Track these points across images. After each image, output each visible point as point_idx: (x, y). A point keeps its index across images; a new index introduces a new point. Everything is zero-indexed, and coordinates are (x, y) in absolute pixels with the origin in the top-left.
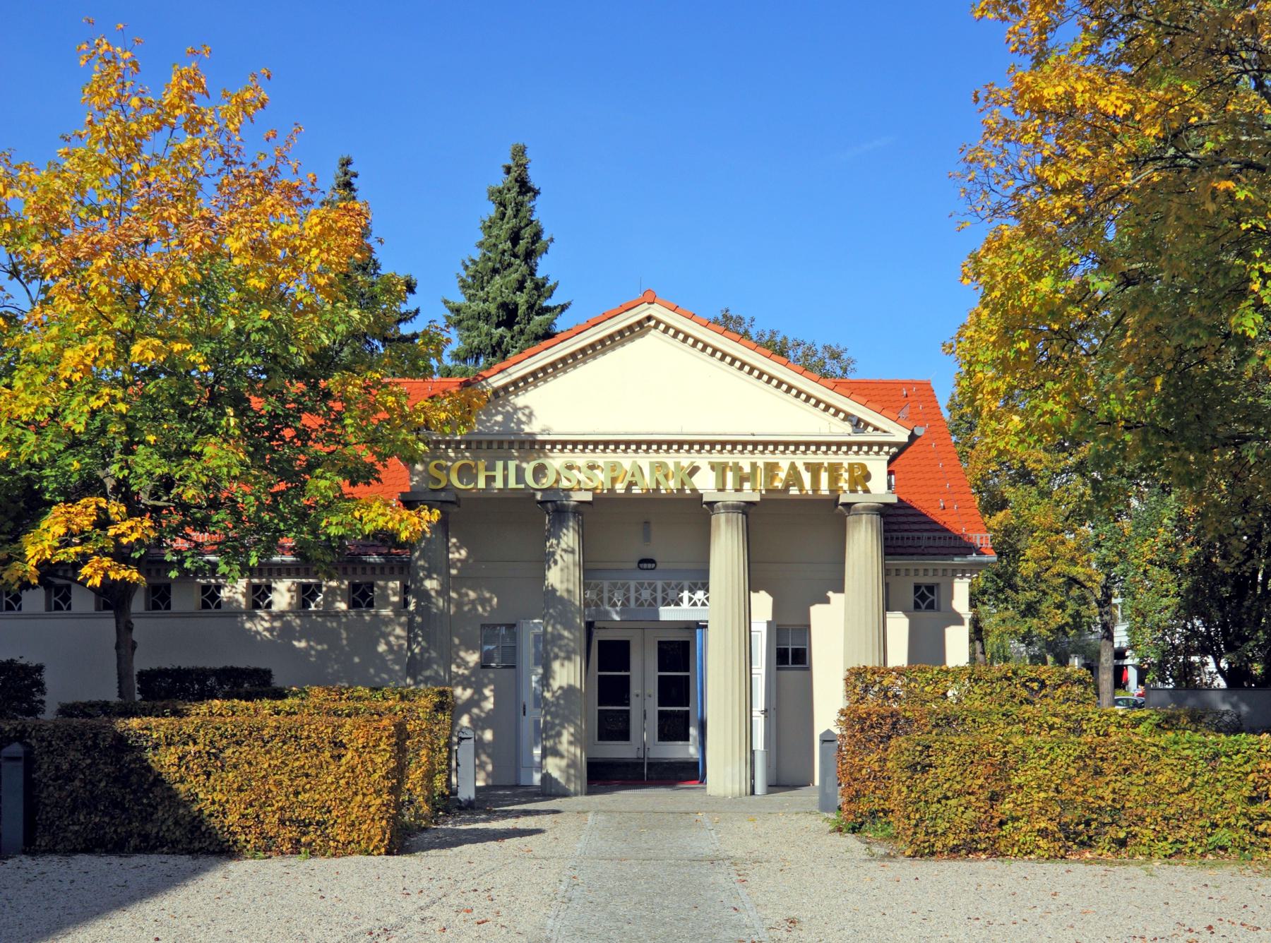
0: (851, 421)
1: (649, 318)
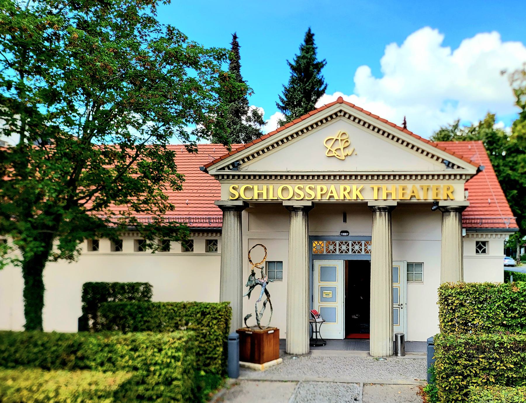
0: (445, 163)
1: (341, 111)
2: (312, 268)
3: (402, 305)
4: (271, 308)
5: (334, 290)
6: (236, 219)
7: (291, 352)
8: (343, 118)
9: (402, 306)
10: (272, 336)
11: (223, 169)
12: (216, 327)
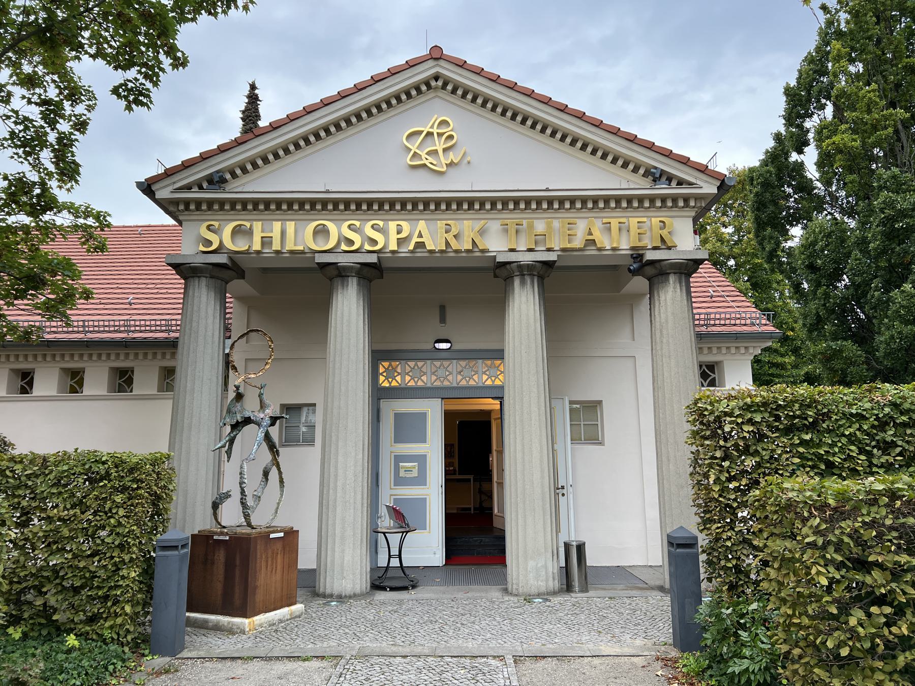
1: (436, 78)
2: (376, 416)
3: (563, 487)
4: (281, 481)
5: (421, 460)
6: (212, 294)
7: (328, 591)
8: (441, 93)
9: (564, 491)
10: (279, 546)
11: (188, 188)
12: (121, 512)
